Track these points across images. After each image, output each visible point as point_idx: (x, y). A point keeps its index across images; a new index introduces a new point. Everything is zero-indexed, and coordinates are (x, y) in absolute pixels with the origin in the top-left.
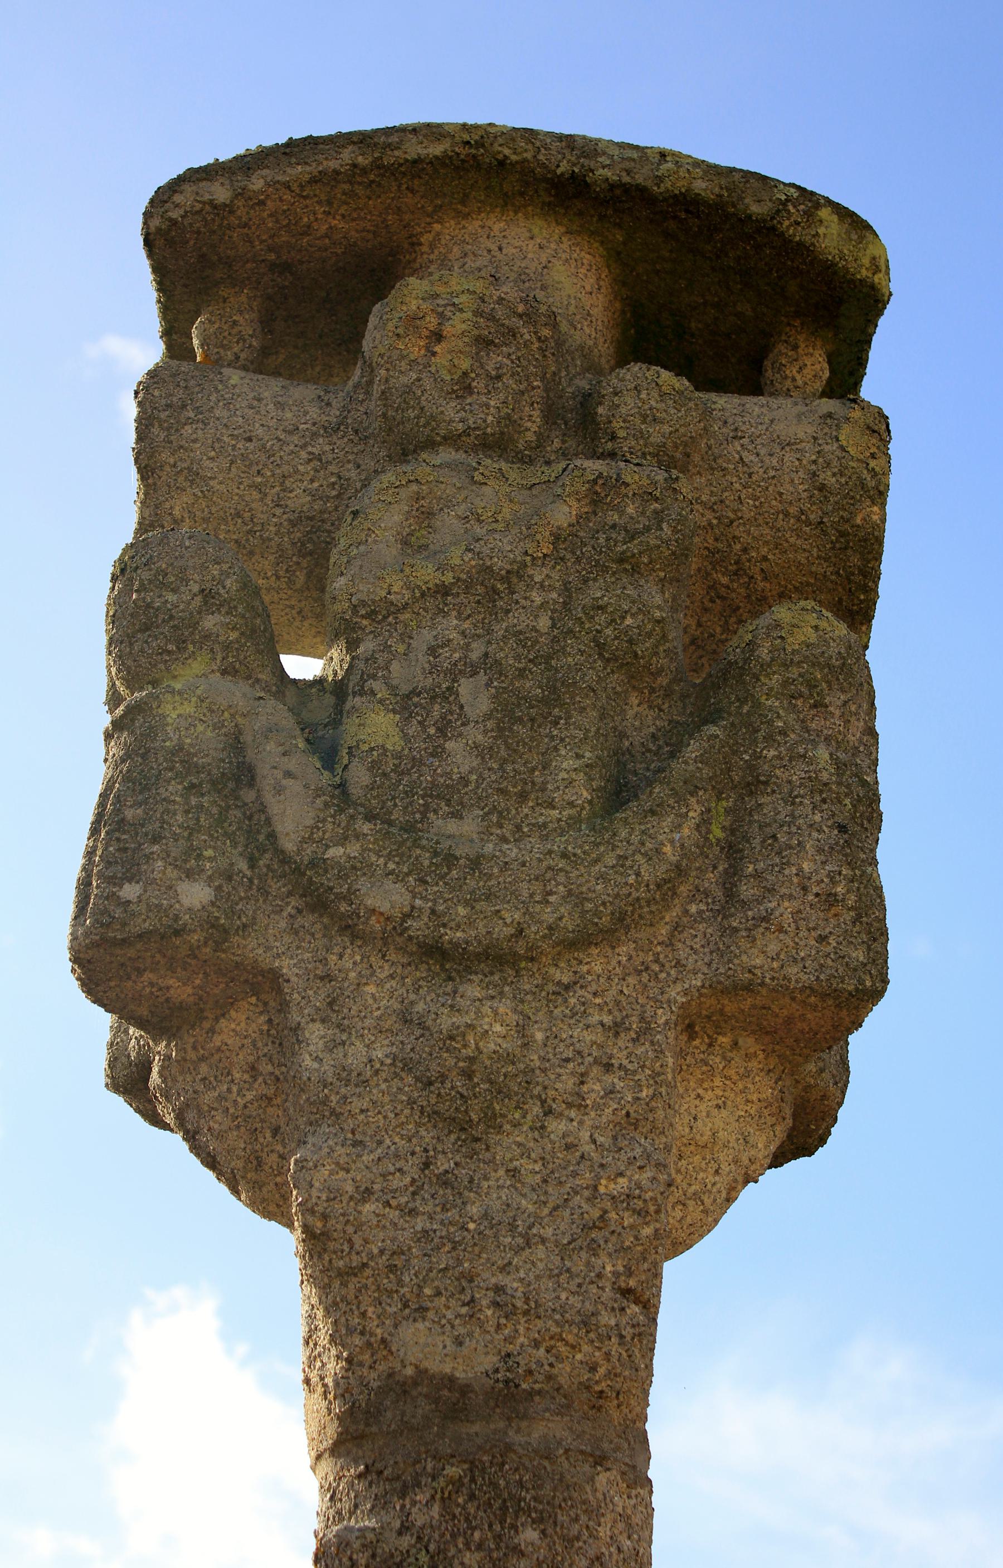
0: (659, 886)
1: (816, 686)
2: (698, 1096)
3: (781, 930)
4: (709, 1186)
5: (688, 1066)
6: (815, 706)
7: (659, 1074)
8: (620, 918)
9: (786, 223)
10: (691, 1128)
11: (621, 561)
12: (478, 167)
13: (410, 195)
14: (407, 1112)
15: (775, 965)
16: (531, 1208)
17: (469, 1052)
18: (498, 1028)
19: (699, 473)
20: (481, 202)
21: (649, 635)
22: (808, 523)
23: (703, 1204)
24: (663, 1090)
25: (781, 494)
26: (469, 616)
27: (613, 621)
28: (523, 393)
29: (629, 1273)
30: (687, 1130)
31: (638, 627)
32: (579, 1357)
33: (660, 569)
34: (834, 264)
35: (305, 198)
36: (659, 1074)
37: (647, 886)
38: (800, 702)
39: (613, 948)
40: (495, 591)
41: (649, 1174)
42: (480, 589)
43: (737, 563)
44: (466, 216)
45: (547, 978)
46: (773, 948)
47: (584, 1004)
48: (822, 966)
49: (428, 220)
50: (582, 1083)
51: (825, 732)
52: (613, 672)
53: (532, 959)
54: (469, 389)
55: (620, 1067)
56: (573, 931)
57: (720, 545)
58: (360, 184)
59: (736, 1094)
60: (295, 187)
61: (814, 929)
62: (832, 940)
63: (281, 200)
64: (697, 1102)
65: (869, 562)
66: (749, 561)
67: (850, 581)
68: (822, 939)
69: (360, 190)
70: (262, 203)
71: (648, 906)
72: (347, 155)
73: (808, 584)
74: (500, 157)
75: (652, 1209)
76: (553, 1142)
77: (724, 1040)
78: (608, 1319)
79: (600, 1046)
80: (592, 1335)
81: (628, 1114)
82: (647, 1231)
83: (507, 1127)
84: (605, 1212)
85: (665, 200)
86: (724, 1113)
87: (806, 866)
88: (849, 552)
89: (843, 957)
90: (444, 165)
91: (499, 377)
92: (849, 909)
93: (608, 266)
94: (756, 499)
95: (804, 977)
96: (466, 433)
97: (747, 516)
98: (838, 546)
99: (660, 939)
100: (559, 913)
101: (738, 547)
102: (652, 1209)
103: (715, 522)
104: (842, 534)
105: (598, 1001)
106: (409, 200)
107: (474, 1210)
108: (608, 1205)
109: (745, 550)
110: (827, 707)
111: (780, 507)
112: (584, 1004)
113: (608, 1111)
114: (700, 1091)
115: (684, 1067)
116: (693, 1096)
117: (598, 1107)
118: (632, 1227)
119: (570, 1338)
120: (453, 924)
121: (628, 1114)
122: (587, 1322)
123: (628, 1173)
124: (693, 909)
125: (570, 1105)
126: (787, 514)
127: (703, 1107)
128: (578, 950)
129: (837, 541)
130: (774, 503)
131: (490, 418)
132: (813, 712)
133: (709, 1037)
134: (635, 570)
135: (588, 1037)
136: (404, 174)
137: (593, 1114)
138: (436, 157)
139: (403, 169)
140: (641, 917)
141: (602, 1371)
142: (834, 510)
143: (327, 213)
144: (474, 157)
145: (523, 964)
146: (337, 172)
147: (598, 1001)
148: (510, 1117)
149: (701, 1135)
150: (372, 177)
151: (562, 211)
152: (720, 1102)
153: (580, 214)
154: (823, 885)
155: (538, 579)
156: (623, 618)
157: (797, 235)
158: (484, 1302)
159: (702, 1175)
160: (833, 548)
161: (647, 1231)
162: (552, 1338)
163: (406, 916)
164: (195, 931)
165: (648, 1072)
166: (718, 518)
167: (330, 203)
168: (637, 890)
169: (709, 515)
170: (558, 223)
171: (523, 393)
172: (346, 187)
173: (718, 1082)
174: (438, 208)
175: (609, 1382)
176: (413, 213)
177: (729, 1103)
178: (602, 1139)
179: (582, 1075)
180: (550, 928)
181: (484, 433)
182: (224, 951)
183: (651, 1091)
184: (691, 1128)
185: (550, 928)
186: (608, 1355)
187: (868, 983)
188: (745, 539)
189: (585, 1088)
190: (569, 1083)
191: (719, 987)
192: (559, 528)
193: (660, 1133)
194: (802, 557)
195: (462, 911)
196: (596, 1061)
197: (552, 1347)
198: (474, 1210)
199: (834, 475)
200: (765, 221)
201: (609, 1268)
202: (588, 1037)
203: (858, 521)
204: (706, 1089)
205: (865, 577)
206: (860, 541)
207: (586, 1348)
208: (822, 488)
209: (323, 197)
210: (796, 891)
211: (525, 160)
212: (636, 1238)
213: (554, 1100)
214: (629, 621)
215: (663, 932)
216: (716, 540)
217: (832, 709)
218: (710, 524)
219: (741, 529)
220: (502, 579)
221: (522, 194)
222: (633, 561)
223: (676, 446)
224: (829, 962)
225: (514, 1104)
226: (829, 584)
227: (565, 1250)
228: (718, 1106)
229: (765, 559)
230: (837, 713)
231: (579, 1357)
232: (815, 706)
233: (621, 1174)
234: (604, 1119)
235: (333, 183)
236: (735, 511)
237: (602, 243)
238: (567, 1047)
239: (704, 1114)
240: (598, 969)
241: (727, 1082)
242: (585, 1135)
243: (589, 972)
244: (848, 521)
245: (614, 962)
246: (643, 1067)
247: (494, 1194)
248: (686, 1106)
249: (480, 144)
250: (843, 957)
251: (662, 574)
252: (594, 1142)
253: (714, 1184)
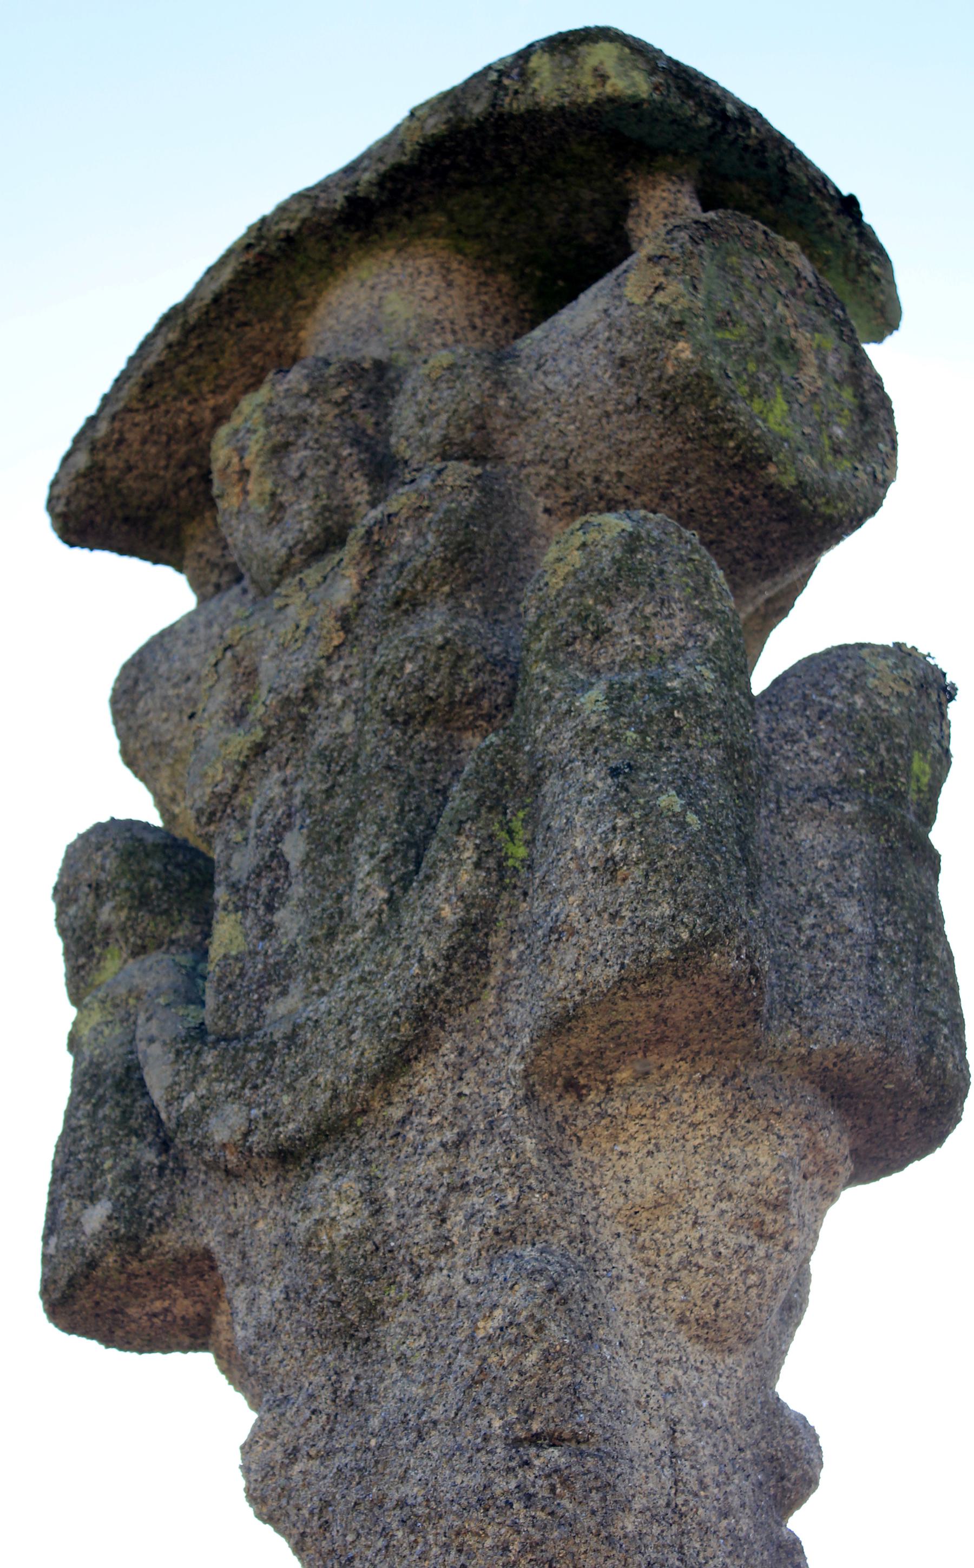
0: (448, 958)
1: (587, 617)
2: (622, 1154)
3: (574, 932)
4: (695, 1245)
5: (585, 1129)
6: (597, 638)
7: (517, 1167)
8: (421, 1017)
9: (507, 100)
10: (626, 1195)
11: (397, 604)
12: (274, 259)
13: (247, 329)
14: (310, 1342)
15: (579, 976)
16: (421, 1392)
17: (326, 1251)
18: (346, 1208)
19: (512, 434)
20: (311, 284)
21: (436, 668)
22: (629, 410)
23: (700, 1267)
24: (533, 1181)
25: (591, 398)
26: (288, 759)
27: (394, 678)
28: (335, 473)
29: (527, 1415)
30: (621, 1200)
31: (421, 668)
32: (489, 1543)
33: (441, 586)
34: (561, 108)
35: (156, 406)
36: (517, 1167)
37: (435, 965)
38: (577, 646)
39: (436, 1051)
40: (303, 718)
41: (521, 1289)
42: (290, 725)
43: (601, 497)
44: (314, 305)
45: (387, 1122)
46: (569, 959)
47: (422, 1132)
48: (623, 947)
49: (290, 334)
50: (443, 1221)
51: (618, 659)
52: (417, 732)
53: (364, 1112)
54: (281, 507)
55: (477, 1181)
56: (378, 1060)
57: (574, 492)
58: (192, 356)
59: (665, 1128)
60: (135, 405)
61: (605, 910)
62: (626, 913)
63: (136, 425)
64: (623, 1162)
65: (708, 405)
66: (608, 487)
67: (705, 438)
68: (614, 916)
69: (198, 361)
70: (121, 441)
71: (448, 985)
72: (160, 343)
73: (674, 470)
74: (282, 235)
75: (530, 1330)
76: (431, 1305)
77: (624, 1075)
78: (504, 1485)
79: (451, 1170)
80: (492, 1512)
81: (497, 1232)
82: (533, 1357)
83: (389, 1311)
84: (485, 1359)
85: (421, 161)
86: (661, 1157)
87: (579, 844)
88: (682, 410)
89: (643, 923)
90: (247, 281)
91: (303, 475)
92: (636, 864)
93: (459, 251)
94: (573, 420)
95: (609, 972)
96: (291, 555)
97: (576, 446)
98: (667, 412)
99: (490, 1010)
100: (366, 1049)
101: (589, 481)
102: (530, 1330)
103: (552, 472)
104: (664, 396)
105: (435, 1120)
106: (252, 334)
107: (375, 1423)
108: (486, 1349)
109: (597, 480)
110: (609, 630)
111: (598, 411)
112: (422, 1132)
113: (475, 1238)
114: (619, 1148)
115: (581, 1134)
116: (615, 1157)
117: (465, 1240)
118: (512, 1362)
119: (473, 1526)
120: (283, 1119)
121: (497, 1232)
122: (484, 1500)
123: (502, 1301)
124: (514, 955)
125: (437, 1253)
126: (607, 415)
127: (631, 1164)
128: (399, 1076)
129: (664, 407)
130: (590, 412)
131: (306, 523)
132: (598, 645)
133: (603, 1082)
134: (415, 604)
135: (432, 1166)
136: (218, 317)
137: (461, 1251)
138: (231, 281)
139: (212, 315)
140: (448, 1002)
141: (515, 1547)
142: (644, 376)
143: (194, 401)
144: (261, 254)
145: (359, 1122)
146: (160, 364)
147: (435, 1120)
148: (386, 1298)
149: (642, 1196)
150: (195, 343)
151: (375, 237)
152: (651, 1147)
153: (391, 226)
154: (598, 855)
155: (336, 677)
156: (402, 669)
157: (520, 105)
158: (394, 1525)
159: (678, 1237)
160: (665, 418)
161: (533, 1357)
162: (458, 1534)
163: (246, 1135)
164: (104, 1255)
165: (505, 1170)
166: (553, 467)
167: (185, 392)
168: (425, 977)
169: (545, 470)
170: (385, 250)
171: (335, 473)
172: (182, 368)
173: (632, 1127)
174: (286, 319)
175: (530, 1556)
176: (269, 340)
177: (663, 1142)
178: (477, 1274)
179: (439, 1213)
180: (357, 1071)
181: (307, 543)
182: (149, 1256)
183: (516, 1190)
184: (626, 1195)
185: (357, 1071)
186: (515, 1527)
187: (685, 936)
188: (588, 468)
189: (448, 1225)
190: (429, 1230)
191: (544, 1032)
192: (344, 608)
193: (553, 1229)
194: (647, 449)
195: (286, 1099)
196: (451, 1189)
197: (462, 1544)
198: (375, 1423)
199: (630, 338)
200: (491, 114)
201: (497, 1423)
202: (432, 1166)
203: (670, 371)
204: (625, 1142)
205: (716, 423)
206: (683, 390)
207: (490, 1530)
208: (623, 362)
209: (173, 393)
210: (575, 878)
211: (304, 221)
212: (521, 1374)
213: (420, 1256)
214: (409, 667)
215: (492, 1000)
216: (567, 489)
217: (616, 629)
218: (550, 478)
219: (580, 460)
220: (303, 701)
221: (333, 250)
222: (407, 597)
223: (461, 429)
224: (629, 939)
225: (384, 1283)
226: (690, 455)
227: (455, 1424)
228: (650, 1153)
229: (620, 475)
230: (625, 628)
231: (489, 1543)
232: (597, 638)
233: (495, 1306)
234: (473, 1250)
235: (167, 375)
236: (563, 448)
237: (436, 235)
238: (417, 1189)
239: (637, 1170)
240: (429, 1083)
241: (644, 1121)
242: (458, 1279)
243: (420, 1094)
244: (660, 378)
245: (440, 1067)
246: (497, 1168)
247: (396, 1389)
248: (610, 1174)
249: (260, 238)
250: (643, 923)
251: (446, 589)
252: (468, 1281)
253: (701, 1238)
